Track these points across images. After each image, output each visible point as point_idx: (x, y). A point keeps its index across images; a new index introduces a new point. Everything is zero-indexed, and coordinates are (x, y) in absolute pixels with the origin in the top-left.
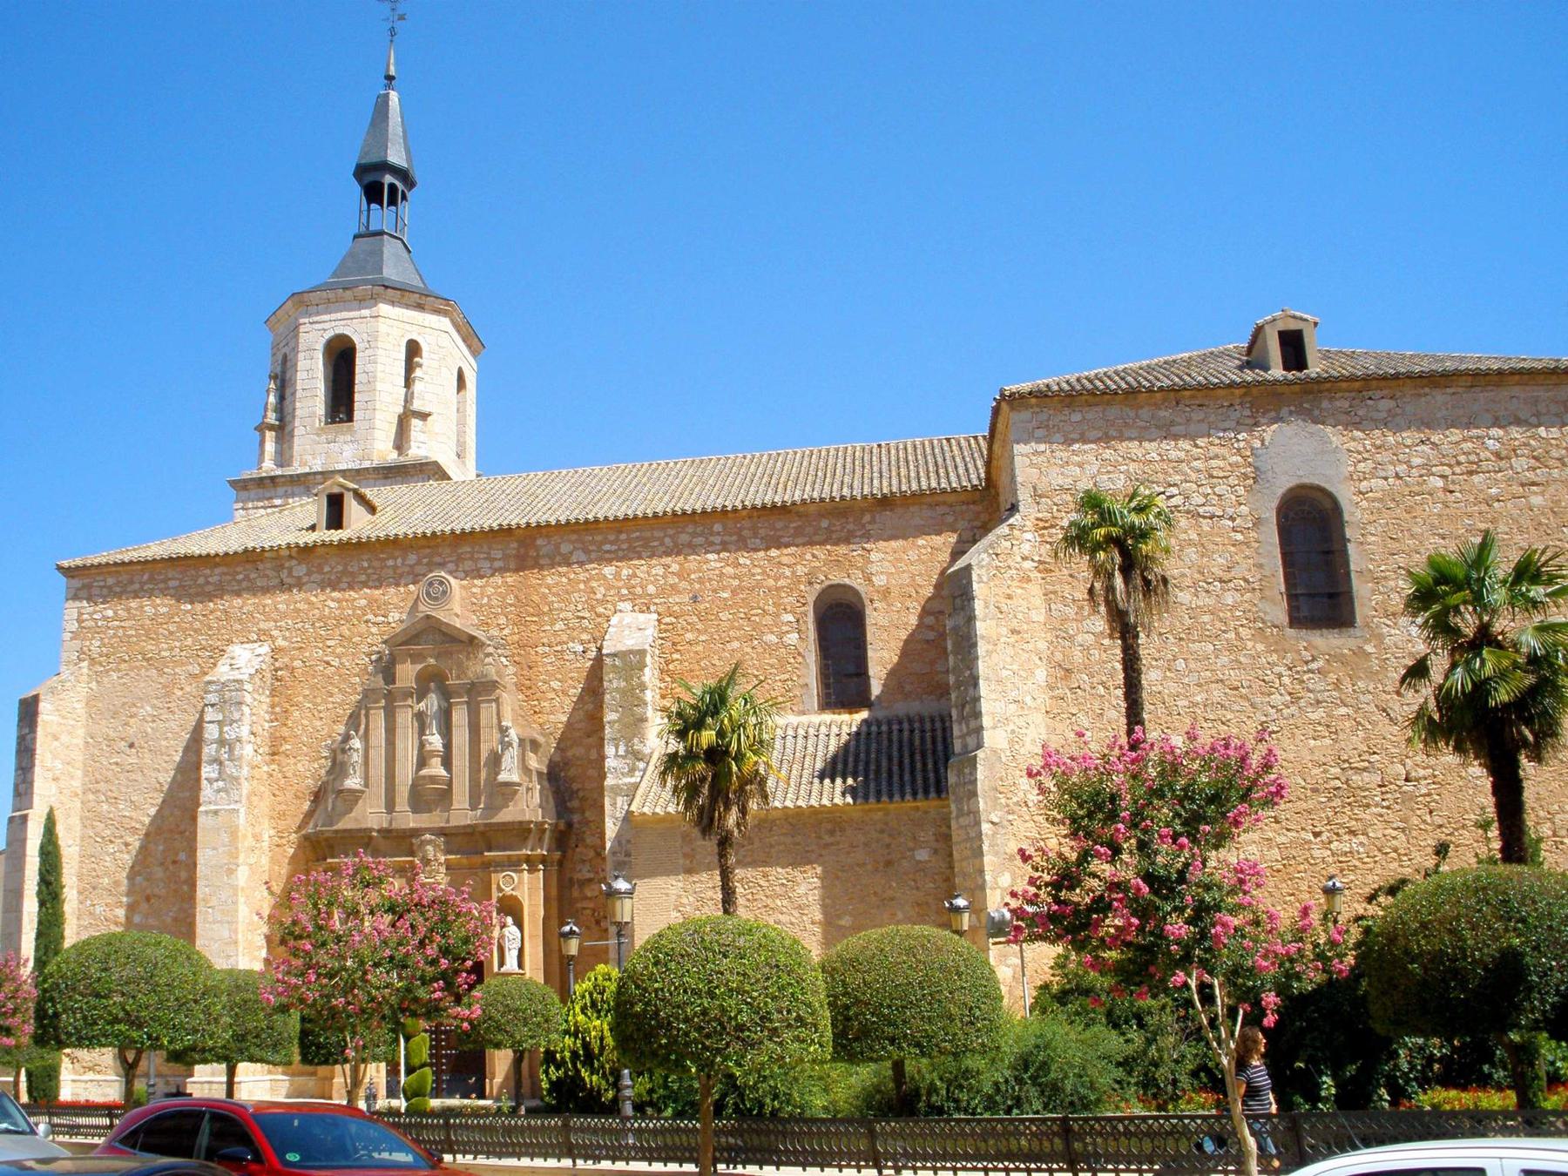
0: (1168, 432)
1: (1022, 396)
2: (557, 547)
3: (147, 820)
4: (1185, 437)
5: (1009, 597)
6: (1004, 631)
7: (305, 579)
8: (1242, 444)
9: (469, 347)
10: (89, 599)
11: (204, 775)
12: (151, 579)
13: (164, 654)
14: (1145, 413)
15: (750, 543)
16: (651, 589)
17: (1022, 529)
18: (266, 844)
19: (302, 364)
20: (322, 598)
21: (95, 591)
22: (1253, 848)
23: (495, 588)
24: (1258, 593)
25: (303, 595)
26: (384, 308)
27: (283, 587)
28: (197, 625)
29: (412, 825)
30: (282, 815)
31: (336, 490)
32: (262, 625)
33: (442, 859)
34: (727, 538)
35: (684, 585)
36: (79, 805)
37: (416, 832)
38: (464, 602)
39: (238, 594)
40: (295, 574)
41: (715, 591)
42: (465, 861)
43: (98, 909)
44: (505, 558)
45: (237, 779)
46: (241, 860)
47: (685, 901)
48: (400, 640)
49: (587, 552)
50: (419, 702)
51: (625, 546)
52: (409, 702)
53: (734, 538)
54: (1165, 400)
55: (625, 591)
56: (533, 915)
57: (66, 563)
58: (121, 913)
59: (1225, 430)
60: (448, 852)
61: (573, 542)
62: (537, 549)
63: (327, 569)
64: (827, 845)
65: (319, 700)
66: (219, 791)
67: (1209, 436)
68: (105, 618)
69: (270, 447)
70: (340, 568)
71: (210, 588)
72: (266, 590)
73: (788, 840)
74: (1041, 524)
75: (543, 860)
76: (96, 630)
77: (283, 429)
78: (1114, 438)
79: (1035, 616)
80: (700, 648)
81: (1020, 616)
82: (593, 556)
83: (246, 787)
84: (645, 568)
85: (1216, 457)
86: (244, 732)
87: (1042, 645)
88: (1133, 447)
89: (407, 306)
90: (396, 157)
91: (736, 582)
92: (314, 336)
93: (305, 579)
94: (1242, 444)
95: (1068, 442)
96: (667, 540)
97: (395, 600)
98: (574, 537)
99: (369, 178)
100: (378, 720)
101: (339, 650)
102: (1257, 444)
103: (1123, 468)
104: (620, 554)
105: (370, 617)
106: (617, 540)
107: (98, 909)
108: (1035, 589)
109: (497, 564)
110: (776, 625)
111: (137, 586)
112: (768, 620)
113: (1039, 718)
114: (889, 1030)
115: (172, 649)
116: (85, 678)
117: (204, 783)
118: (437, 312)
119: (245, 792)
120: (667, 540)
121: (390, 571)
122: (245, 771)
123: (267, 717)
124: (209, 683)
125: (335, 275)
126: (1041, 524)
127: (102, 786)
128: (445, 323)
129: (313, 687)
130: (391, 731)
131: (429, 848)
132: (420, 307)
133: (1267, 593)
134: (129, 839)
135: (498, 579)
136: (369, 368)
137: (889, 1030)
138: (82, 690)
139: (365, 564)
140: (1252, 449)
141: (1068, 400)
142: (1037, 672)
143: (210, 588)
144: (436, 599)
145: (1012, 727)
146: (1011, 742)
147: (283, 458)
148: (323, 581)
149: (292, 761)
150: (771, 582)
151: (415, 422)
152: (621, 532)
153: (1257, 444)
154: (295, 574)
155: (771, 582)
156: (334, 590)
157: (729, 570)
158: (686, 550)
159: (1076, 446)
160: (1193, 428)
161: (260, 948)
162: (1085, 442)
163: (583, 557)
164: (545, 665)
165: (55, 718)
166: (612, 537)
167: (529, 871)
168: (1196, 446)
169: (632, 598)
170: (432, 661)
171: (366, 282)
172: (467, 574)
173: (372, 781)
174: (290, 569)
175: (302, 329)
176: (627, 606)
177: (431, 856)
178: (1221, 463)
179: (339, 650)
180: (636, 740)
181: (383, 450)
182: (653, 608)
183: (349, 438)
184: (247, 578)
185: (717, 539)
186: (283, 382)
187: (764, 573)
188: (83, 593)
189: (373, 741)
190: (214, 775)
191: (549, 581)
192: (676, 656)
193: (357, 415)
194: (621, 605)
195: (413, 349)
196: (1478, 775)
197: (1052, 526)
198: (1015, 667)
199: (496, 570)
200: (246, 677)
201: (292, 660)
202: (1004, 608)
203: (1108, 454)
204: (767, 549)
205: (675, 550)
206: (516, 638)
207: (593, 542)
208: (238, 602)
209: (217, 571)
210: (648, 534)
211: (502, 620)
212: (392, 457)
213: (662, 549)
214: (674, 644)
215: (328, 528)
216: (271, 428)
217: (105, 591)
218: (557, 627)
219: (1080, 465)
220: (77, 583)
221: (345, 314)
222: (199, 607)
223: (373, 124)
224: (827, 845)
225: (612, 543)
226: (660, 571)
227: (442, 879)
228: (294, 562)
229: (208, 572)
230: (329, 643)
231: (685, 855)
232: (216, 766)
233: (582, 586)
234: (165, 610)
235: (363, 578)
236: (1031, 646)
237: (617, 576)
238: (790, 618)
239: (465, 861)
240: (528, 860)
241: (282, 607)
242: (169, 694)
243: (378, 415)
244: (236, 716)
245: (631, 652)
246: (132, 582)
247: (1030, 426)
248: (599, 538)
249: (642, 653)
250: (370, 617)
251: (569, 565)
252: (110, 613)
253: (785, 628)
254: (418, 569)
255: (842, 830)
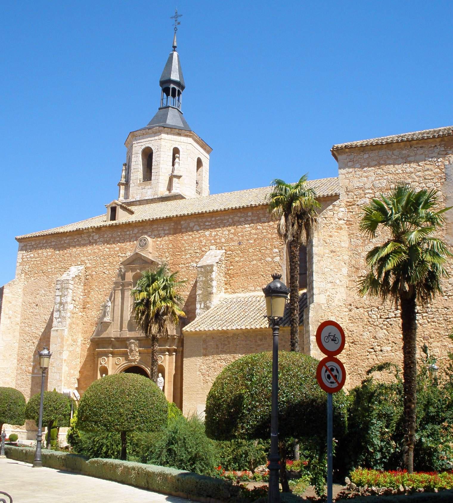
0: (407, 161)
1: (342, 148)
2: (189, 224)
3: (41, 334)
4: (414, 162)
5: (331, 236)
6: (327, 251)
7: (98, 240)
8: (440, 164)
9: (205, 149)
10: (26, 250)
11: (54, 316)
12: (46, 242)
13: (49, 270)
14: (396, 152)
15: (262, 219)
16: (223, 240)
17: (339, 206)
18: (79, 344)
19: (133, 159)
20: (103, 247)
21: (28, 247)
22: (437, 350)
23: (165, 241)
24: (445, 232)
25: (97, 246)
26: (164, 136)
27: (91, 243)
28: (61, 259)
29: (128, 336)
30: (86, 332)
31: (114, 205)
32: (82, 259)
33: (137, 350)
34: (253, 218)
35: (236, 238)
36: (19, 328)
37: (128, 339)
38: (154, 248)
39: (75, 247)
40: (95, 238)
41: (247, 240)
42: (146, 351)
43: (23, 367)
44: (169, 230)
45: (65, 317)
46: (65, 348)
47: (202, 367)
48: (127, 263)
49: (200, 226)
50: (134, 287)
51: (214, 223)
52: (130, 287)
53: (256, 218)
54: (405, 146)
55: (213, 241)
56: (169, 373)
57: (18, 237)
58: (31, 369)
59: (432, 158)
60: (140, 347)
61: (194, 222)
62: (181, 225)
63: (106, 236)
64: (259, 346)
65: (101, 287)
66: (59, 322)
67: (425, 161)
68: (31, 257)
69: (122, 192)
70: (110, 235)
71: (65, 245)
72: (84, 245)
73: (244, 343)
74: (348, 204)
75: (175, 351)
76: (27, 262)
77: (127, 185)
78: (382, 164)
79: (343, 244)
80: (241, 264)
81: (336, 245)
82: (202, 227)
83: (68, 321)
84: (221, 232)
85: (428, 170)
86: (69, 299)
87: (346, 258)
88: (391, 168)
89: (174, 134)
90: (175, 76)
91: (256, 236)
92: (138, 148)
93: (98, 240)
94: (440, 164)
95: (362, 167)
96: (230, 220)
97: (129, 248)
98: (195, 220)
99: (166, 86)
100: (119, 295)
101: (109, 267)
102: (447, 163)
103: (385, 177)
104: (212, 226)
105: (120, 254)
106: (211, 220)
107: (23, 367)
108: (344, 233)
109: (167, 232)
110: (271, 254)
111: (41, 245)
112: (268, 252)
113: (343, 290)
114: (95, 418)
115: (52, 269)
116: (23, 280)
117: (54, 319)
118: (186, 136)
119: (68, 323)
120: (230, 220)
121: (128, 236)
122: (69, 314)
123: (82, 294)
124: (58, 281)
125: (149, 124)
126: (348, 204)
127: (27, 321)
128: (190, 140)
129: (99, 282)
130: (123, 299)
131: (133, 345)
132: (179, 134)
133: (449, 231)
134: (34, 341)
135: (166, 238)
136: (158, 159)
137: (95, 418)
138: (21, 285)
139: (119, 234)
140: (445, 165)
141: (362, 149)
142: (343, 269)
143: (65, 245)
144: (142, 246)
145: (328, 293)
146: (328, 301)
147: (127, 196)
148: (104, 241)
149: (90, 311)
150: (270, 236)
151: (175, 180)
152: (213, 217)
153: (447, 163)
154: (95, 238)
155: (270, 236)
156: (108, 244)
157: (254, 231)
158: (237, 224)
159: (365, 169)
160: (418, 157)
161: (74, 384)
162: (369, 167)
163: (198, 228)
164: (182, 272)
165: (10, 295)
166: (209, 219)
167: (169, 355)
168: (419, 166)
169: (216, 244)
170: (138, 271)
171: (156, 126)
172: (155, 236)
173: (115, 318)
174: (93, 236)
175: (134, 146)
176: (213, 247)
177: (133, 349)
178: (430, 173)
179: (109, 267)
180: (208, 302)
181: (163, 191)
182: (223, 248)
183: (149, 187)
184: (78, 240)
185: (249, 219)
186: (128, 166)
187: (267, 232)
188: (24, 248)
189: (116, 303)
190: (58, 316)
191: (185, 238)
192: (231, 267)
193: (153, 178)
194: (212, 247)
195: (176, 151)
196: (391, 308)
197: (353, 205)
198: (332, 267)
199: (166, 234)
200: (70, 278)
201: (92, 271)
202: (328, 241)
203: (379, 171)
204: (269, 222)
205: (234, 224)
206: (172, 261)
207: (201, 222)
208: (74, 250)
209: (68, 238)
210: (223, 218)
211: (167, 254)
212: (166, 193)
213: (228, 223)
214: (231, 262)
215: (111, 220)
216: (123, 184)
217: (31, 247)
218: (187, 257)
219: (367, 177)
220: (22, 244)
221: (150, 139)
222: (61, 252)
223: (167, 65)
224: (259, 346)
225: (209, 222)
226: (227, 232)
227: (137, 358)
228: (94, 234)
229: (65, 238)
230: (105, 265)
231: (204, 349)
232: (58, 313)
233: (197, 240)
234: (50, 253)
235: (118, 239)
236: (340, 258)
237: (210, 235)
238: (277, 250)
239: (146, 351)
240: (168, 350)
241: (89, 251)
242: (50, 286)
243: (161, 177)
244: (66, 293)
245: (208, 266)
246: (40, 243)
247: (346, 161)
248: (204, 220)
249: (212, 266)
250: (120, 254)
251: (193, 231)
252: (32, 255)
253: (274, 255)
254: (137, 235)
255: (266, 339)
